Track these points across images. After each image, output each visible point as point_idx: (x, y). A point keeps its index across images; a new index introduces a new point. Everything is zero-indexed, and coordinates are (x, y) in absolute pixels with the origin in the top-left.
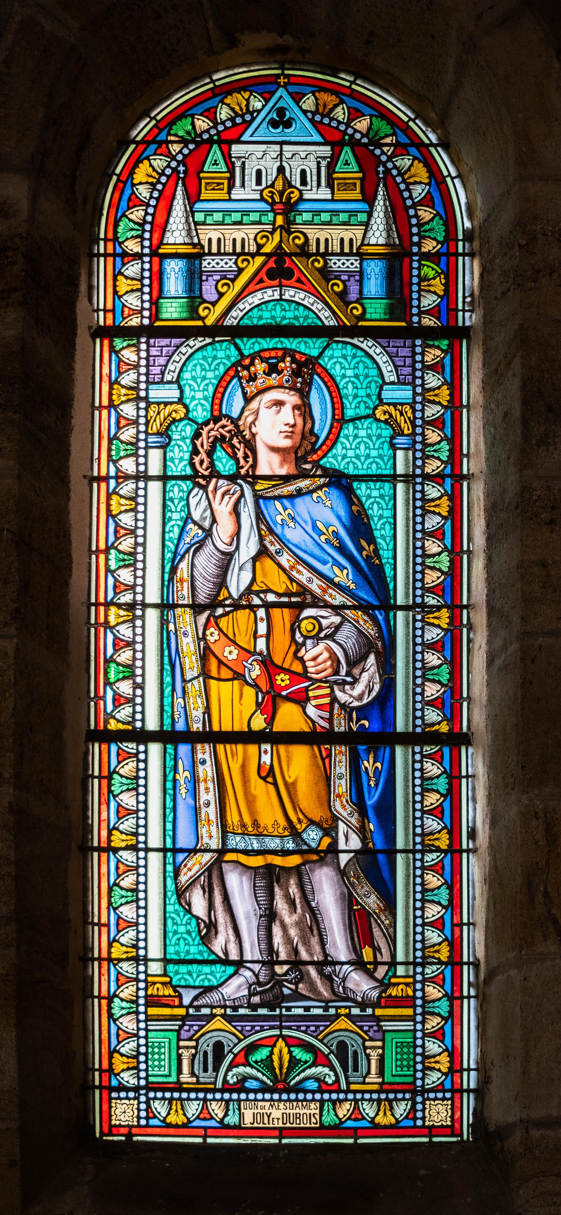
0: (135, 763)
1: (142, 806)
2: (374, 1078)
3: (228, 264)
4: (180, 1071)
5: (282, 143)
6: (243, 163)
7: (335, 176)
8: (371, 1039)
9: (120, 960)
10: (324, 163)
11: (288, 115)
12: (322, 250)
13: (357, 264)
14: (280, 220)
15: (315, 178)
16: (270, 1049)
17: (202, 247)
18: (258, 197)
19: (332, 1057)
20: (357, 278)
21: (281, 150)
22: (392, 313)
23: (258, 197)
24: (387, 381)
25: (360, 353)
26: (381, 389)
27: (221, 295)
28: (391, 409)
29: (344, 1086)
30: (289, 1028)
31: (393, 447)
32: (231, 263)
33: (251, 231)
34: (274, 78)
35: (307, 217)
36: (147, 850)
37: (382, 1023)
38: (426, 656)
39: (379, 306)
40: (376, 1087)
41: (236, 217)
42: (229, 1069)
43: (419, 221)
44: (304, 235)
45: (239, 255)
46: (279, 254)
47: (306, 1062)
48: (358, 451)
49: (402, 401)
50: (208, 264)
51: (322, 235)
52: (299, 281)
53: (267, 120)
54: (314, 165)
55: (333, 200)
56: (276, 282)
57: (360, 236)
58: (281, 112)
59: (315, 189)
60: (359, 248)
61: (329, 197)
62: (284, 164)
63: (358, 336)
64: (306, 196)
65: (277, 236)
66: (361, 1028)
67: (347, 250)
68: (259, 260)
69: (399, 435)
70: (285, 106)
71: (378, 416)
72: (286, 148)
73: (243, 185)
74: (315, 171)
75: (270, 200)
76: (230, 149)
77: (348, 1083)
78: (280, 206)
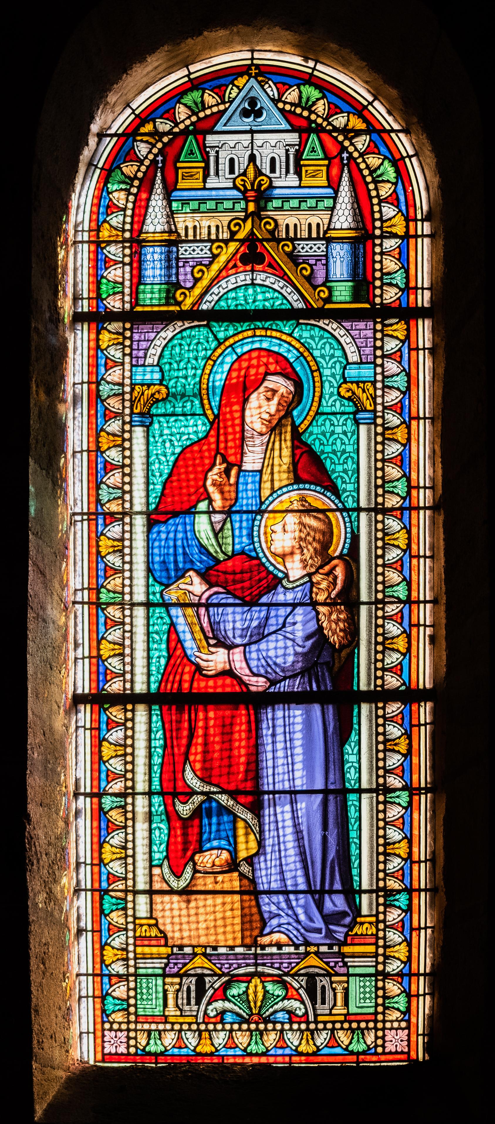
0: (122, 684)
1: (127, 567)
2: (340, 1009)
3: (202, 251)
4: (165, 1005)
5: (252, 132)
6: (217, 152)
7: (302, 163)
8: (337, 974)
9: (108, 604)
10: (292, 151)
11: (259, 106)
12: (292, 234)
13: (323, 248)
14: (252, 207)
15: (284, 165)
16: (246, 984)
17: (179, 235)
18: (231, 185)
19: (301, 991)
20: (324, 262)
21: (252, 139)
22: (356, 296)
23: (231, 185)
24: (350, 360)
25: (327, 335)
26: (345, 368)
27: (196, 280)
28: (354, 387)
29: (311, 1018)
30: (264, 965)
31: (357, 423)
32: (206, 250)
33: (225, 219)
34: (245, 68)
35: (277, 203)
36: (133, 605)
37: (346, 960)
38: (388, 728)
39: (343, 288)
40: (342, 1018)
41: (211, 205)
42: (209, 1003)
43: (384, 993)
44: (275, 221)
45: (213, 242)
46: (251, 240)
47: (278, 996)
48: (323, 351)
49: (364, 379)
50: (185, 250)
51: (292, 221)
52: (270, 265)
53: (240, 109)
54: (282, 152)
55: (300, 187)
56: (248, 268)
57: (326, 221)
58: (253, 102)
59: (283, 176)
60: (325, 232)
61: (297, 184)
62: (255, 152)
63: (324, 318)
64: (276, 183)
65: (249, 222)
66: (327, 963)
67: (314, 235)
68: (233, 246)
69: (362, 411)
70: (256, 95)
71: (342, 394)
72: (256, 136)
73: (217, 174)
74: (283, 159)
75: (242, 188)
76: (205, 139)
77: (316, 1016)
78: (252, 194)
